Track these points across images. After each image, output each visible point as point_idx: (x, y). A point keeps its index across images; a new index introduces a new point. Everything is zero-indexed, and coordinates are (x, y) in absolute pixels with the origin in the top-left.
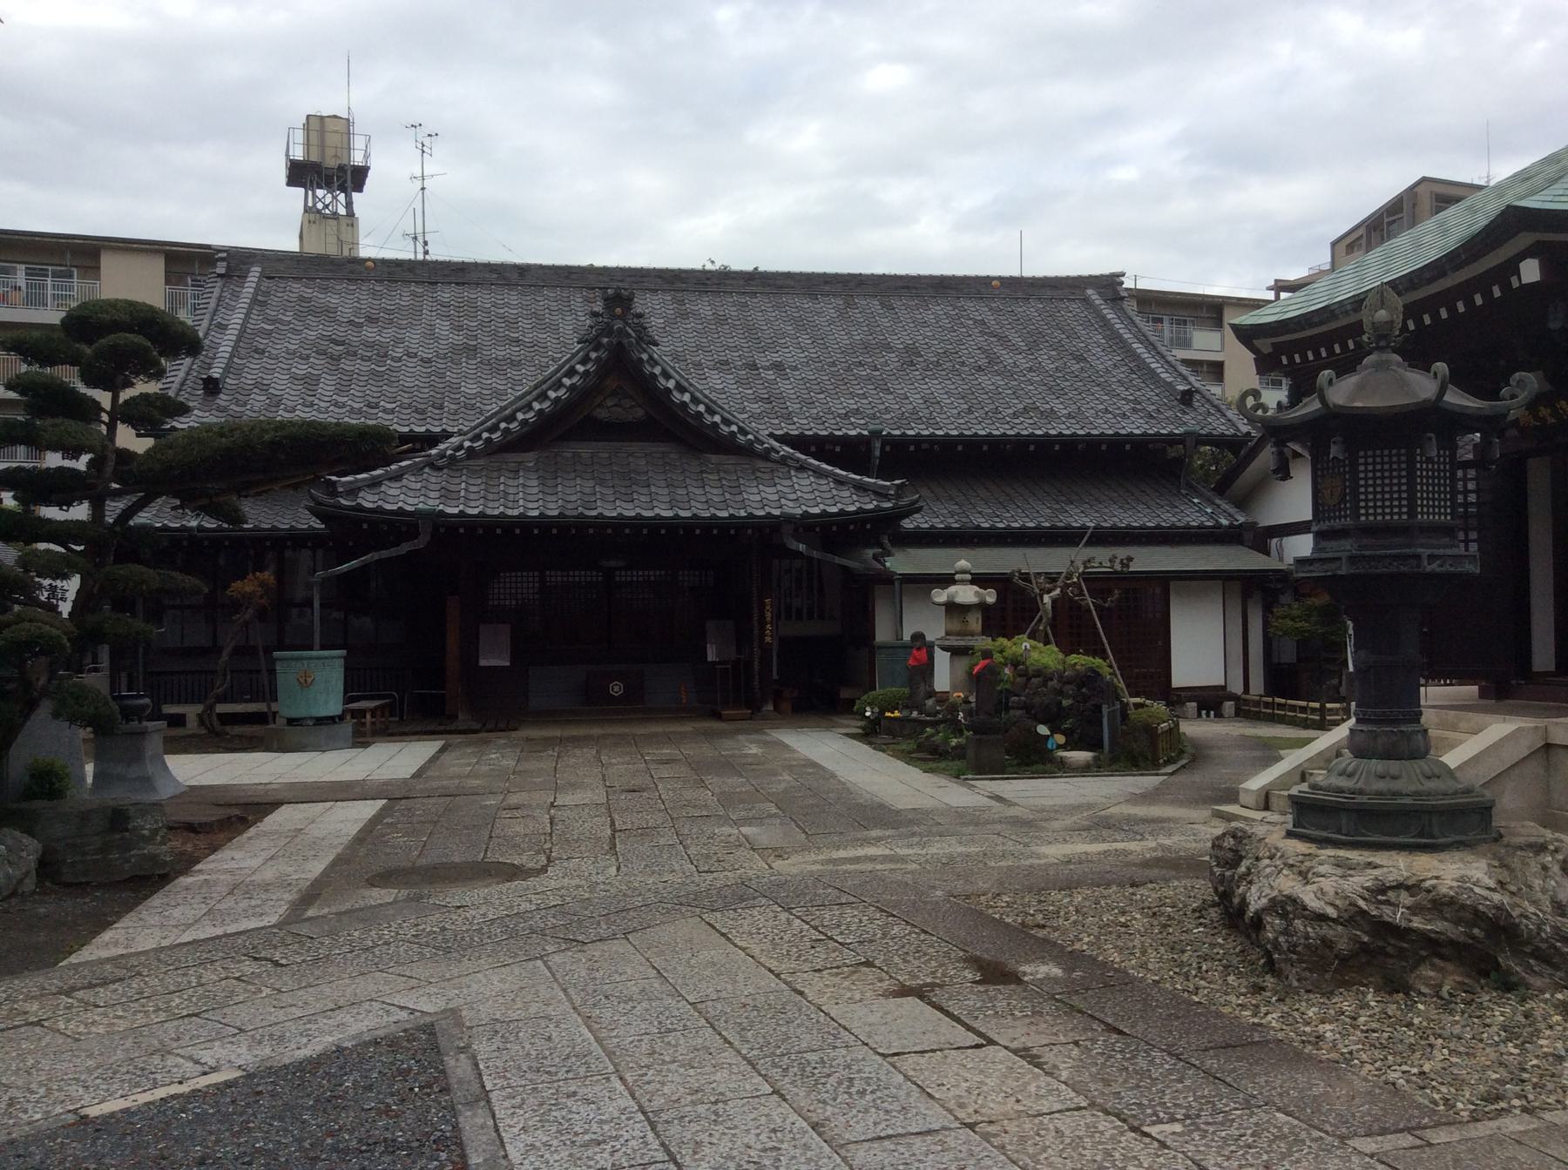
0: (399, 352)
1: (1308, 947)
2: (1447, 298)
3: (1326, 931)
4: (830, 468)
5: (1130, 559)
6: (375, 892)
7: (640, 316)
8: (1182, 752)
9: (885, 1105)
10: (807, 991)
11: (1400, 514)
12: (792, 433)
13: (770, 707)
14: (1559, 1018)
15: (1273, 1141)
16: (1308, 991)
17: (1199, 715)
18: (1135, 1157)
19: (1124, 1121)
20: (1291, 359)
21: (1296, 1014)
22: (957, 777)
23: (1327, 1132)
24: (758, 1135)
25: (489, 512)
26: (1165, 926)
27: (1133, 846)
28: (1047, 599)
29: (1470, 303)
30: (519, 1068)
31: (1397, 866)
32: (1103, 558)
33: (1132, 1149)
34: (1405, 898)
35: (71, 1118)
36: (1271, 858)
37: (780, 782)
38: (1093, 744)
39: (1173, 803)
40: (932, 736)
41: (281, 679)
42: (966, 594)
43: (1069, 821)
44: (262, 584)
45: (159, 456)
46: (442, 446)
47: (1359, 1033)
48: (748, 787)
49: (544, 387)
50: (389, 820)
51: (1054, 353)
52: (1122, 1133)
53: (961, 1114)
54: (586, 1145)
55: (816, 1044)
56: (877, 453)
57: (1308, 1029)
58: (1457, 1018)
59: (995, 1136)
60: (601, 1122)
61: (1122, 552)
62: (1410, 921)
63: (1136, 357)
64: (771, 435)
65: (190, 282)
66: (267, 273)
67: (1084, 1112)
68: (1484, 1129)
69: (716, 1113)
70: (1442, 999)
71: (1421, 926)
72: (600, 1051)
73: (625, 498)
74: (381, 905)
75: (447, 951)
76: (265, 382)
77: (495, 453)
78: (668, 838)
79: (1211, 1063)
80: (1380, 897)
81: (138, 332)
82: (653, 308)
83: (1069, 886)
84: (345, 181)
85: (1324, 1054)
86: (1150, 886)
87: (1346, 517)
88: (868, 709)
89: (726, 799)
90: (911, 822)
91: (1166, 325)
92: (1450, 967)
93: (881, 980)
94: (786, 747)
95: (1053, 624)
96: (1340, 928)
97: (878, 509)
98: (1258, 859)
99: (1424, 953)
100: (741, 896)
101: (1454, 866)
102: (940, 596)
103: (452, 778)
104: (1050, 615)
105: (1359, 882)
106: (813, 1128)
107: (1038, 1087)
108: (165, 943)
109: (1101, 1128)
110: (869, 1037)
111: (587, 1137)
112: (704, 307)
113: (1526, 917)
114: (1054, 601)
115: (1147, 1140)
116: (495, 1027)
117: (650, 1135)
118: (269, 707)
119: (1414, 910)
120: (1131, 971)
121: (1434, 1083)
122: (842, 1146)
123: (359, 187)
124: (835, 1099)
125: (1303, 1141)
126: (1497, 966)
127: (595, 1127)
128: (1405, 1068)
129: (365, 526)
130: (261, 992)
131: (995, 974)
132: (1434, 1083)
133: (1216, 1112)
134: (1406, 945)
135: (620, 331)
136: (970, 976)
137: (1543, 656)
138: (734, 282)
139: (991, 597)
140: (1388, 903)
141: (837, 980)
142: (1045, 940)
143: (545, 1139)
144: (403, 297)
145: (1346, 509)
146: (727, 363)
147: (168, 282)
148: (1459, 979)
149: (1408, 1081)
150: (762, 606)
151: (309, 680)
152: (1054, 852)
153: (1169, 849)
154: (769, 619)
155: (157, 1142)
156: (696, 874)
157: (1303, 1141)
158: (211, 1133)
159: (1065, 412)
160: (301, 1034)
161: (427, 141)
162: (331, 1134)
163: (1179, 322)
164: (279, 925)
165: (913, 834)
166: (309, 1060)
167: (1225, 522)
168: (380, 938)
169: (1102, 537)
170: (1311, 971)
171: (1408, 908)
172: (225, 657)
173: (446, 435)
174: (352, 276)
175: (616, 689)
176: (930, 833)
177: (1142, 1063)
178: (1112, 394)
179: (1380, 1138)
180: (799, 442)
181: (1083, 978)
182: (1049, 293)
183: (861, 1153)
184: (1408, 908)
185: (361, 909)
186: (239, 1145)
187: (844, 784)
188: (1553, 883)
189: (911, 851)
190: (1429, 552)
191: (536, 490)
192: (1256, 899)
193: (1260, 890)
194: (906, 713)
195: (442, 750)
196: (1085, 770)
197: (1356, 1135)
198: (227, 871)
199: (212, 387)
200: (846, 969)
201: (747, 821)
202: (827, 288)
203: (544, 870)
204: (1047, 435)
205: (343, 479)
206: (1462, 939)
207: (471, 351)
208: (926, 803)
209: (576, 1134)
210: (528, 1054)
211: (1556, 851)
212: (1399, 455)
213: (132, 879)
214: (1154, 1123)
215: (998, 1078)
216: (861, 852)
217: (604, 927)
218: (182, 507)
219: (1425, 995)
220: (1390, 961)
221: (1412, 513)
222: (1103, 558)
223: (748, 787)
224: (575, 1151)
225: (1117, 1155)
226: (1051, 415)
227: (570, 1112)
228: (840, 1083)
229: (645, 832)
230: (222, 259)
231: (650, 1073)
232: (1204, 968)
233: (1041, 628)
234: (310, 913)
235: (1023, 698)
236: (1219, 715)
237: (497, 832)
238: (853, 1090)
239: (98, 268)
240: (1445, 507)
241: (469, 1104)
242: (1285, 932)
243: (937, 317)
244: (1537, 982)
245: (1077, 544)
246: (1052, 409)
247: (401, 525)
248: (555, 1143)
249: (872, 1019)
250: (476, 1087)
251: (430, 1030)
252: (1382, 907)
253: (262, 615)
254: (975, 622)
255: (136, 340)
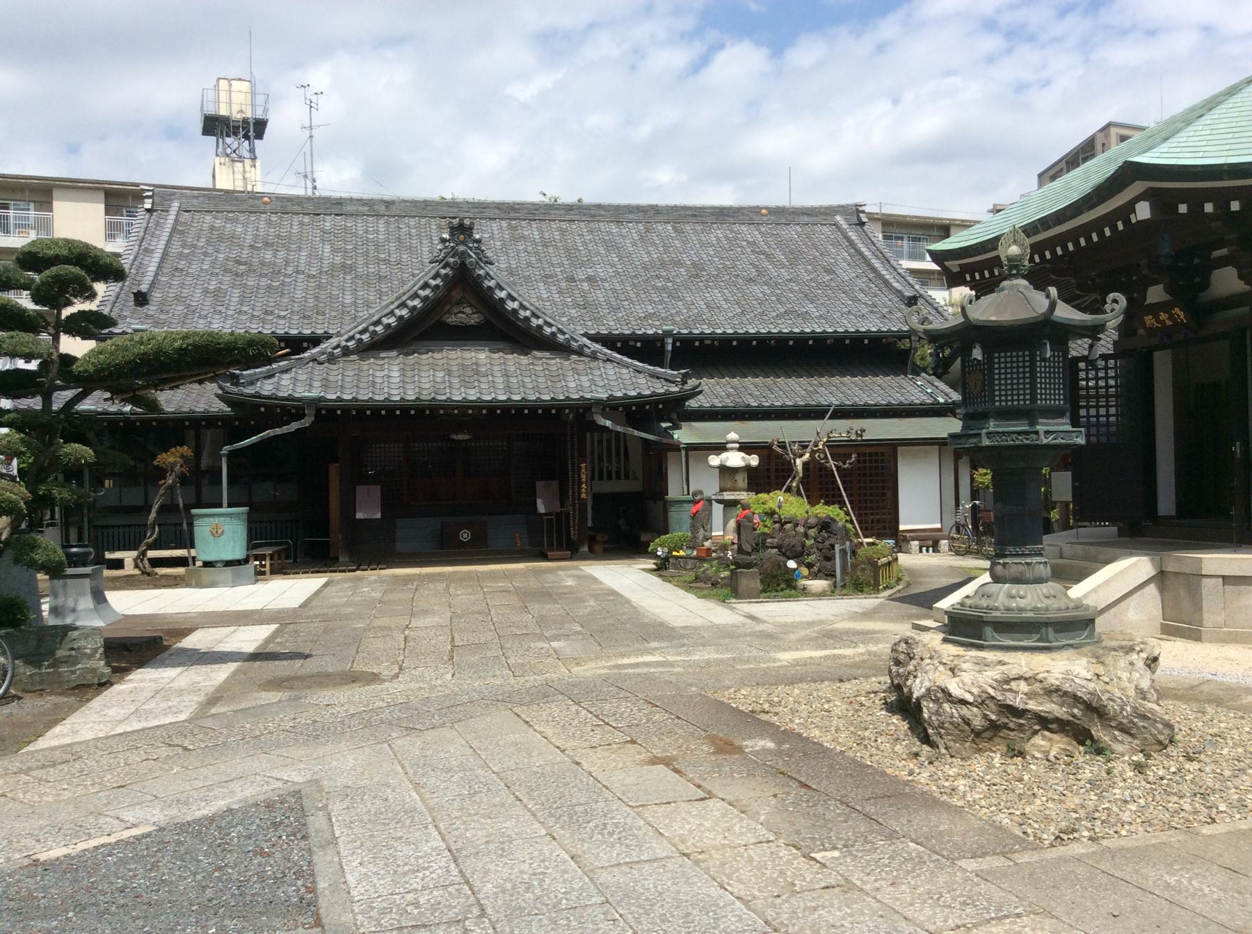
0: (290, 270)
1: (952, 723)
2: (1061, 239)
3: (965, 711)
4: (630, 360)
5: (863, 431)
6: (264, 695)
7: (479, 241)
8: (899, 580)
9: (628, 841)
10: (583, 762)
11: (1025, 400)
12: (602, 332)
13: (586, 549)
14: (1132, 774)
15: (903, 863)
16: (952, 757)
17: (921, 551)
18: (801, 875)
19: (798, 849)
20: (973, 277)
21: (939, 773)
22: (724, 602)
23: (943, 856)
24: (531, 864)
25: (361, 397)
26: (857, 711)
27: (848, 652)
28: (799, 462)
29: (1114, 228)
30: (361, 821)
31: (1021, 663)
32: (842, 429)
33: (800, 869)
34: (1023, 687)
35: (26, 862)
36: (931, 658)
37: (586, 607)
38: (830, 575)
39: (884, 619)
40: (707, 570)
41: (197, 530)
42: (735, 459)
43: (802, 633)
44: (182, 456)
45: (93, 360)
46: (323, 346)
47: (983, 786)
48: (562, 611)
49: (415, 288)
50: (279, 640)
51: (810, 267)
52: (795, 858)
53: (682, 847)
54: (405, 874)
55: (582, 800)
56: (669, 348)
57: (947, 784)
58: (1059, 775)
59: (704, 861)
60: (417, 858)
61: (857, 424)
62: (1026, 704)
63: (874, 270)
64: (586, 335)
65: (125, 213)
66: (184, 207)
67: (771, 844)
68: (1061, 851)
69: (503, 849)
70: (1048, 760)
71: (1034, 708)
72: (423, 807)
73: (468, 385)
74: (268, 704)
75: (317, 737)
76: (184, 295)
77: (364, 351)
78: (495, 652)
79: (870, 809)
80: (1005, 686)
81: (75, 265)
82: (488, 233)
83: (792, 681)
84: (249, 131)
85: (955, 801)
86: (854, 681)
87: (985, 402)
88: (659, 549)
89: (542, 621)
90: (683, 636)
91: (905, 242)
92: (1056, 737)
93: (640, 754)
94: (595, 580)
95: (803, 481)
96: (975, 709)
97: (667, 393)
98: (922, 659)
99: (1037, 727)
100: (544, 694)
101: (1062, 663)
102: (714, 460)
103: (330, 608)
104: (801, 475)
105: (993, 674)
106: (572, 858)
107: (742, 827)
108: (101, 735)
109: (781, 854)
110: (623, 794)
111: (406, 868)
112: (532, 231)
113: (1113, 700)
114: (805, 464)
115: (812, 863)
116: (346, 793)
117: (453, 866)
118: (189, 553)
119: (1030, 695)
120: (825, 744)
121: (1030, 821)
122: (591, 871)
123: (260, 135)
124: (591, 838)
125: (925, 862)
126: (1091, 737)
127: (412, 860)
128: (1011, 811)
129: (262, 409)
130: (172, 769)
131: (725, 747)
132: (1030, 821)
133: (866, 841)
134: (1023, 722)
135: (463, 253)
136: (706, 749)
137: (1166, 503)
138: (557, 212)
139: (754, 461)
140: (1011, 690)
141: (607, 754)
142: (767, 723)
143: (375, 870)
144: (293, 225)
145: (985, 396)
146: (551, 276)
147: (107, 213)
148: (1062, 746)
149: (1011, 820)
150: (580, 469)
151: (220, 531)
152: (786, 657)
153: (875, 654)
154: (584, 480)
155: (90, 877)
156: (512, 678)
157: (925, 862)
158: (130, 870)
159: (817, 314)
160: (201, 800)
161: (314, 98)
162: (219, 869)
163: (914, 240)
164: (189, 721)
165: (683, 645)
166: (206, 818)
167: (941, 400)
168: (266, 729)
169: (842, 413)
170: (955, 742)
171: (1026, 694)
172: (153, 515)
173: (328, 337)
174: (252, 209)
175: (465, 535)
176: (696, 645)
177: (820, 809)
178: (855, 300)
179: (980, 860)
180: (609, 341)
181: (788, 749)
182: (806, 219)
183: (605, 875)
184: (1026, 694)
185: (254, 708)
186: (150, 878)
187: (635, 608)
188: (1137, 675)
189: (679, 658)
190: (1046, 428)
191: (397, 380)
192: (918, 688)
193: (922, 683)
194: (689, 552)
195: (325, 585)
196: (821, 595)
197: (964, 857)
198: (151, 680)
199: (141, 299)
200: (615, 746)
201: (556, 638)
202: (631, 216)
203: (397, 676)
204: (802, 332)
205: (244, 373)
206: (1065, 717)
207: (346, 269)
208: (697, 622)
209: (398, 866)
210: (369, 811)
211: (1141, 651)
212: (1024, 356)
213: (79, 687)
214: (820, 851)
215: (713, 821)
216: (640, 659)
217: (437, 717)
218: (111, 399)
219: (1037, 759)
220: (1012, 734)
221: (1034, 399)
222: (842, 429)
223: (562, 611)
224: (396, 877)
225: (789, 873)
226: (805, 316)
227: (396, 851)
228: (596, 827)
229: (480, 647)
230: (148, 197)
231: (458, 823)
232: (879, 740)
233: (794, 484)
234: (213, 711)
235: (776, 540)
236: (936, 550)
237: (362, 647)
238: (605, 832)
239: (50, 203)
240: (1059, 394)
241: (323, 847)
242: (937, 713)
243: (718, 239)
244: (1119, 748)
245: (823, 418)
246: (807, 312)
247: (288, 409)
248: (382, 872)
249: (628, 781)
250: (328, 835)
251: (297, 794)
252: (1006, 693)
253: (183, 479)
254: (742, 480)
255: (73, 270)
